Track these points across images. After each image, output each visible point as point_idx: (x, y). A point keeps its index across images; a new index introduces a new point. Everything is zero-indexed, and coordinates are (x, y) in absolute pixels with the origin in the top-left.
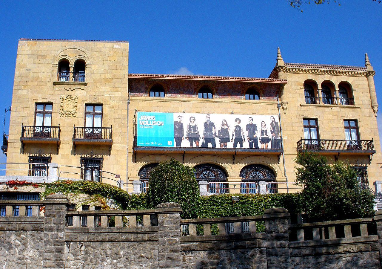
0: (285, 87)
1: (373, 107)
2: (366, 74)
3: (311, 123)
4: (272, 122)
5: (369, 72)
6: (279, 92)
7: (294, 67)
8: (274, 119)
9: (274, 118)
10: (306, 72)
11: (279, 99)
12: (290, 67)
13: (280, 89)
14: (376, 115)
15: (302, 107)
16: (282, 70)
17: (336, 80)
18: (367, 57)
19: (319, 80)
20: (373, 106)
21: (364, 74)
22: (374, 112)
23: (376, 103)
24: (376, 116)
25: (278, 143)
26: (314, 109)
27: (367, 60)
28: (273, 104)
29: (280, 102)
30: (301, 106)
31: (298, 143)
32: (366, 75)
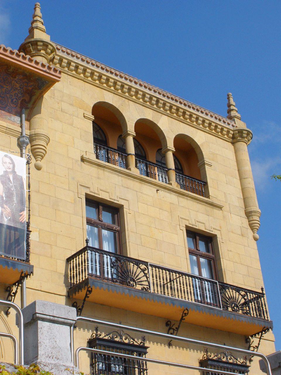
0: (47, 96)
1: (248, 214)
2: (233, 135)
3: (105, 211)
4: (6, 172)
5: (241, 132)
6: (30, 105)
7: (74, 59)
8: (11, 166)
9: (13, 163)
10: (101, 81)
11: (26, 124)
12: (65, 55)
13: (34, 98)
14: (257, 236)
15: (85, 166)
16: (43, 52)
17: (170, 128)
18: (232, 102)
19: (132, 113)
20: (251, 212)
21: (228, 132)
22: (252, 228)
23: (255, 206)
24: (256, 239)
25: (18, 242)
26: (117, 179)
27: (232, 107)
28: (8, 131)
29: (26, 132)
30: (83, 160)
31: (69, 260)
32: (233, 138)
